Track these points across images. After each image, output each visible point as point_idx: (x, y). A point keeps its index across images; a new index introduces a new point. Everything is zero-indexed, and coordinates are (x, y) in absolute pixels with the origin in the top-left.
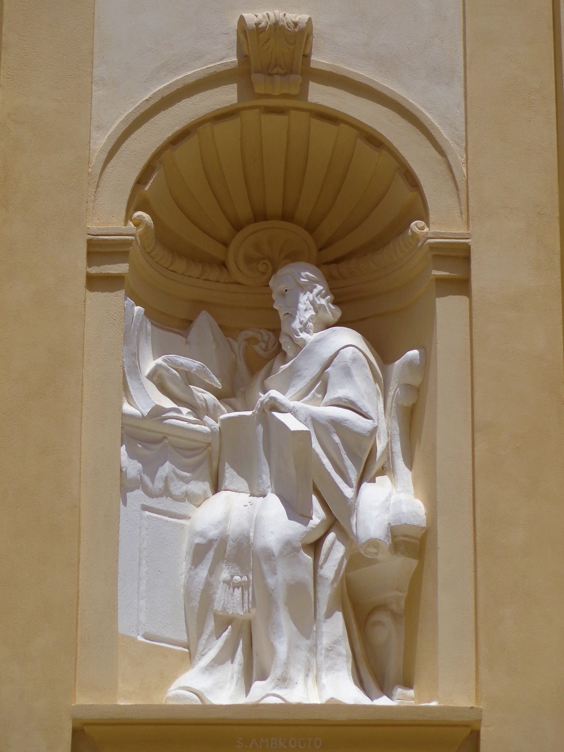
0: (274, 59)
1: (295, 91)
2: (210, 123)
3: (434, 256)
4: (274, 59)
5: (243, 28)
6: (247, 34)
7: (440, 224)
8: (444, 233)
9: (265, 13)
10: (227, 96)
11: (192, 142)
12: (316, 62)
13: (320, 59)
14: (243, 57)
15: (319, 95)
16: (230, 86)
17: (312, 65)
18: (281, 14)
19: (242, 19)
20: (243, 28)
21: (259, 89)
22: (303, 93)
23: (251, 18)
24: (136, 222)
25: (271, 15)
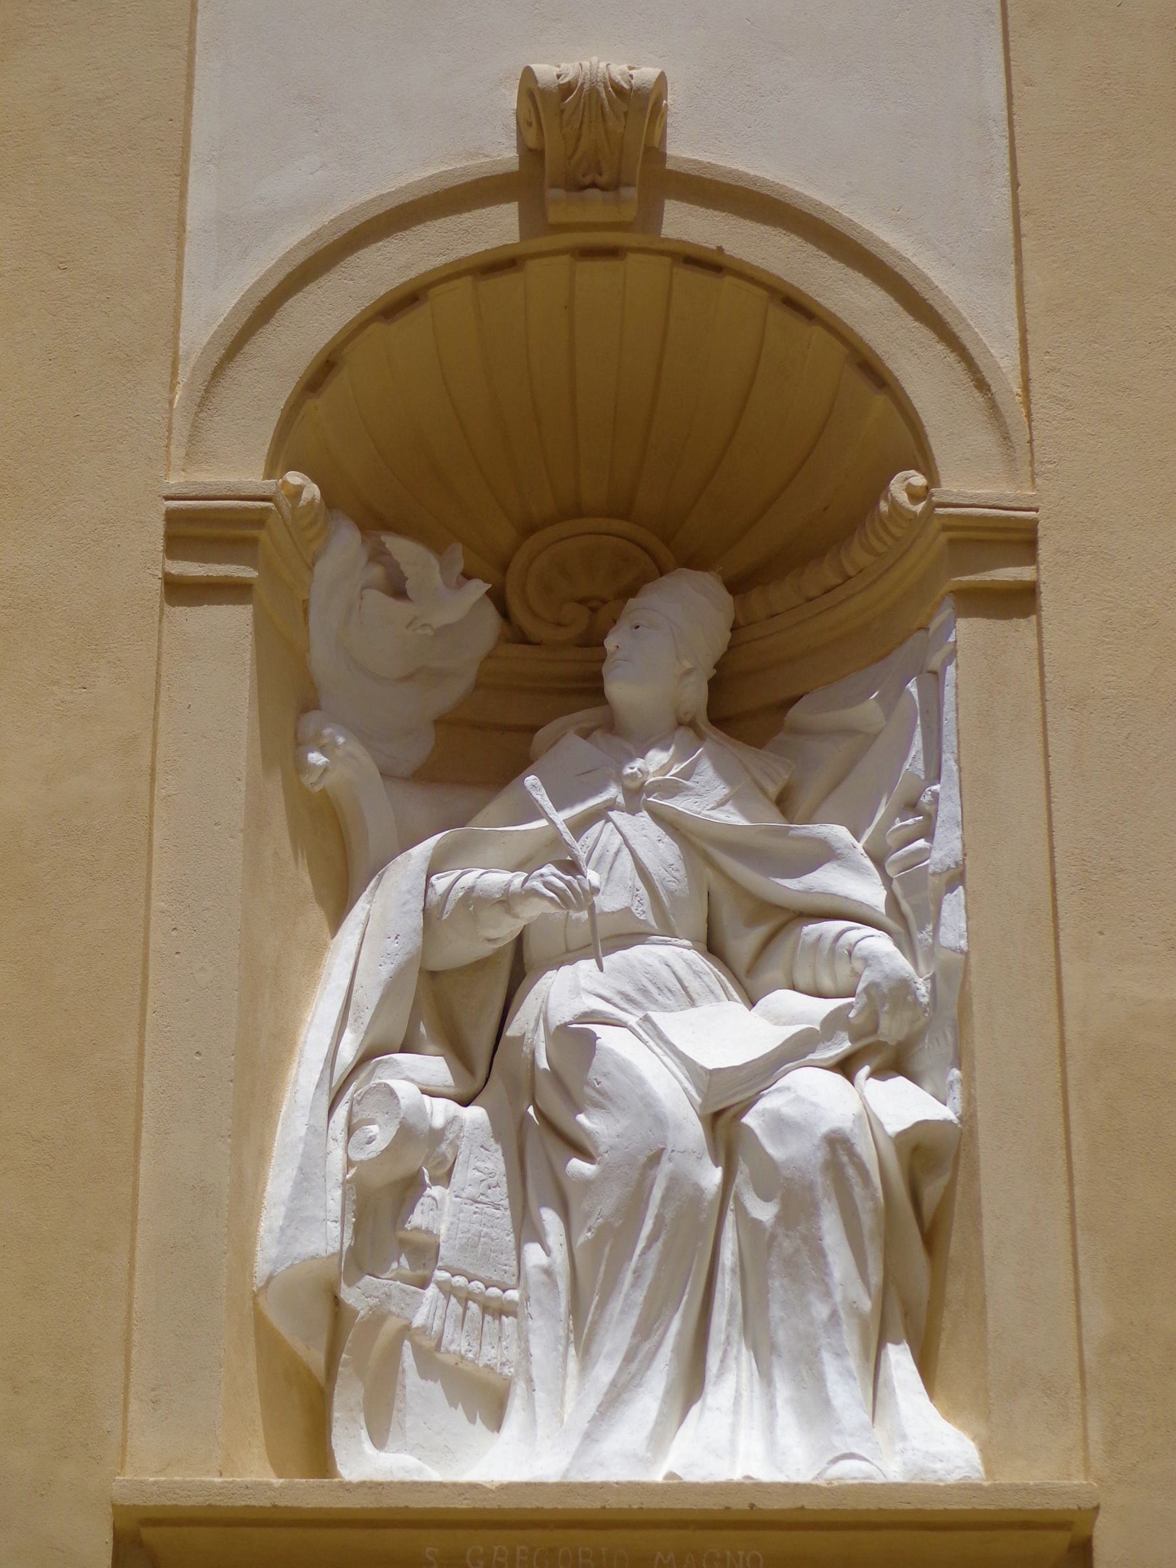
0: (590, 153)
1: (629, 213)
2: (469, 278)
3: (951, 541)
4: (590, 153)
5: (532, 94)
6: (542, 105)
7: (970, 478)
8: (1017, 498)
9: (577, 64)
10: (499, 227)
11: (418, 317)
12: (677, 159)
13: (685, 146)
14: (531, 154)
15: (683, 223)
16: (504, 206)
17: (669, 166)
18: (603, 65)
19: (528, 73)
20: (532, 94)
21: (555, 215)
22: (651, 217)
23: (546, 72)
24: (634, 785)
25: (586, 64)
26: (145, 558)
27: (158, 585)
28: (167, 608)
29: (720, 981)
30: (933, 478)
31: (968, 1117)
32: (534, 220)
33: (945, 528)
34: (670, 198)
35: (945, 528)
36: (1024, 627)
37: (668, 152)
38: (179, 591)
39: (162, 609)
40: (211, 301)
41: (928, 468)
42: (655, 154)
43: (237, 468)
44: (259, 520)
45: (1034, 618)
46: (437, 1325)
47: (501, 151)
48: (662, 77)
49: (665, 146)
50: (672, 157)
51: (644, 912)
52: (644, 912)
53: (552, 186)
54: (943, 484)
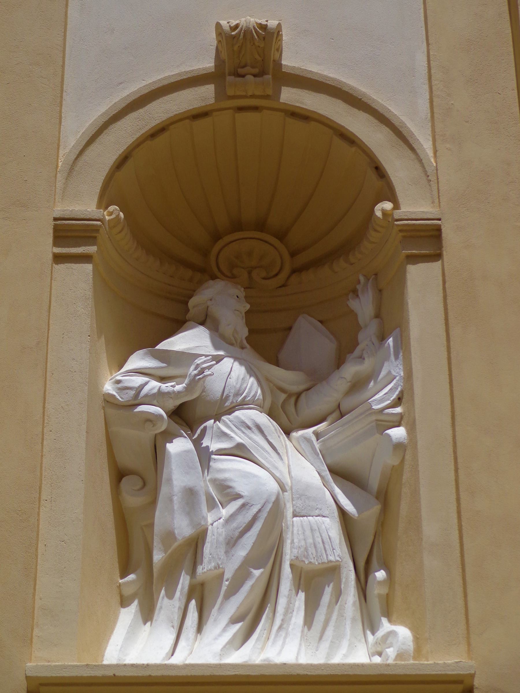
3: (404, 237)
7: (413, 205)
10: (204, 95)
13: (290, 60)
15: (289, 96)
21: (230, 92)
26: (47, 247)
27: (51, 256)
28: (54, 265)
29: (269, 420)
30: (397, 206)
31: (52, 248)
32: (220, 94)
33: (401, 231)
34: (284, 86)
35: (401, 231)
36: (437, 265)
37: (283, 62)
38: (58, 259)
39: (52, 266)
40: (74, 128)
41: (393, 198)
42: (278, 64)
43: (84, 204)
44: (96, 229)
45: (440, 262)
46: (310, 541)
47: (207, 63)
48: (279, 25)
49: (281, 60)
50: (285, 65)
51: (374, 482)
52: (374, 482)
53: (230, 75)
54: (402, 206)
